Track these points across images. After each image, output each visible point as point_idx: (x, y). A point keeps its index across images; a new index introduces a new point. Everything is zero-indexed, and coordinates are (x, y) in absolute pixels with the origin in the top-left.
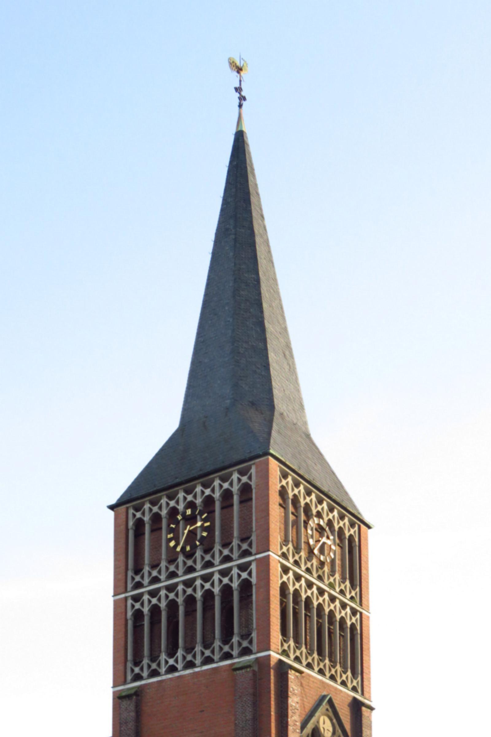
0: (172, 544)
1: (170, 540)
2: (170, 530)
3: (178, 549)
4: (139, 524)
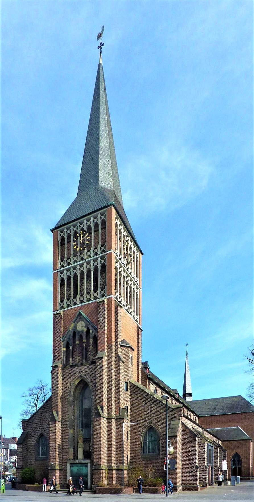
0: (75, 247)
1: (74, 245)
2: (74, 241)
3: (78, 250)
4: (63, 239)
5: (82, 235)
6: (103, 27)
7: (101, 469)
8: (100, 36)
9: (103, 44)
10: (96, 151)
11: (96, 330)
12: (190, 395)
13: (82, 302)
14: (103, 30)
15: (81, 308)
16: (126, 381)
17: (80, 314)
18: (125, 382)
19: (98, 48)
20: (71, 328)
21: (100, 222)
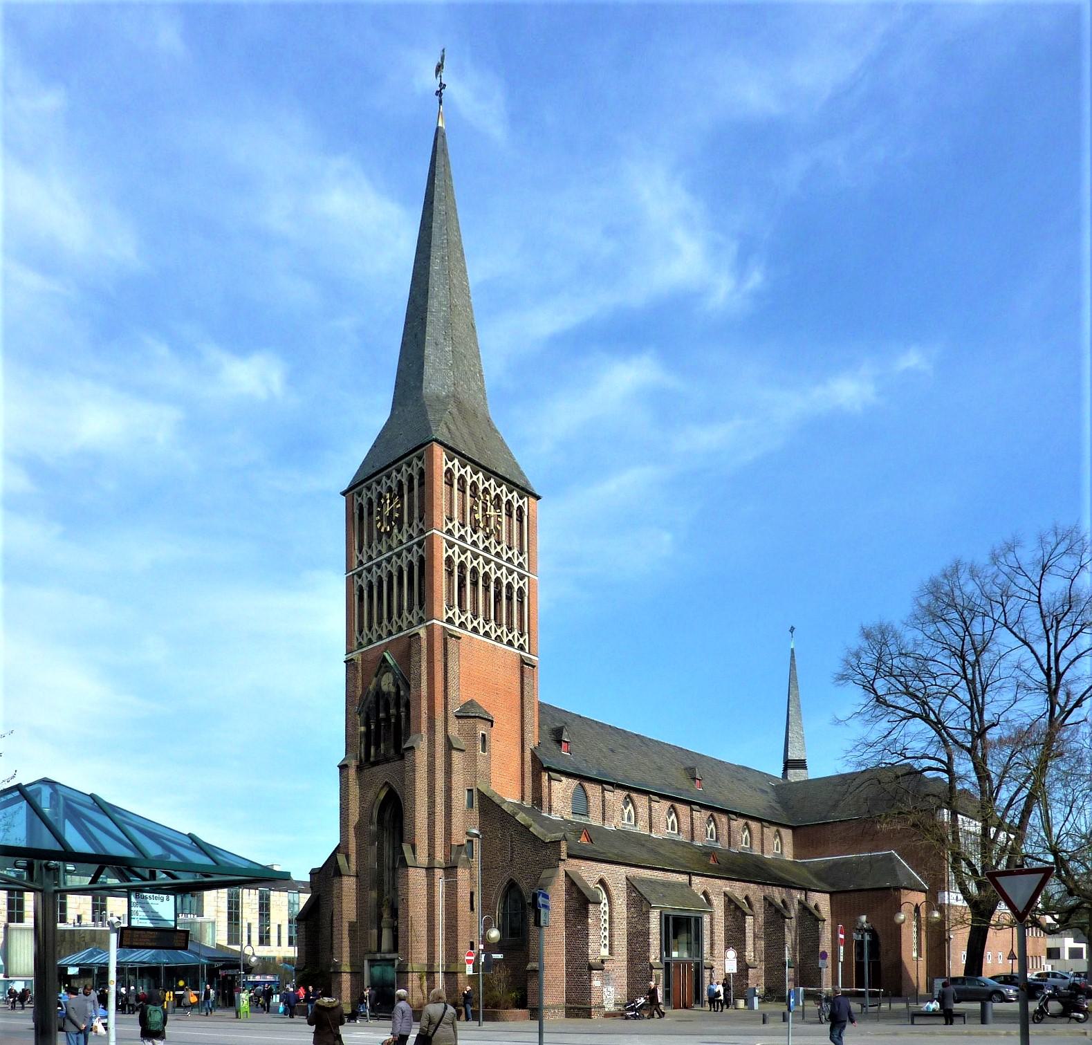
0: (379, 525)
1: (378, 521)
5: (388, 501)
6: (443, 51)
7: (408, 972)
9: (445, 85)
11: (408, 686)
12: (801, 764)
13: (390, 633)
14: (443, 58)
15: (386, 647)
16: (469, 788)
17: (385, 660)
18: (469, 790)
19: (436, 95)
20: (371, 687)
21: (407, 480)
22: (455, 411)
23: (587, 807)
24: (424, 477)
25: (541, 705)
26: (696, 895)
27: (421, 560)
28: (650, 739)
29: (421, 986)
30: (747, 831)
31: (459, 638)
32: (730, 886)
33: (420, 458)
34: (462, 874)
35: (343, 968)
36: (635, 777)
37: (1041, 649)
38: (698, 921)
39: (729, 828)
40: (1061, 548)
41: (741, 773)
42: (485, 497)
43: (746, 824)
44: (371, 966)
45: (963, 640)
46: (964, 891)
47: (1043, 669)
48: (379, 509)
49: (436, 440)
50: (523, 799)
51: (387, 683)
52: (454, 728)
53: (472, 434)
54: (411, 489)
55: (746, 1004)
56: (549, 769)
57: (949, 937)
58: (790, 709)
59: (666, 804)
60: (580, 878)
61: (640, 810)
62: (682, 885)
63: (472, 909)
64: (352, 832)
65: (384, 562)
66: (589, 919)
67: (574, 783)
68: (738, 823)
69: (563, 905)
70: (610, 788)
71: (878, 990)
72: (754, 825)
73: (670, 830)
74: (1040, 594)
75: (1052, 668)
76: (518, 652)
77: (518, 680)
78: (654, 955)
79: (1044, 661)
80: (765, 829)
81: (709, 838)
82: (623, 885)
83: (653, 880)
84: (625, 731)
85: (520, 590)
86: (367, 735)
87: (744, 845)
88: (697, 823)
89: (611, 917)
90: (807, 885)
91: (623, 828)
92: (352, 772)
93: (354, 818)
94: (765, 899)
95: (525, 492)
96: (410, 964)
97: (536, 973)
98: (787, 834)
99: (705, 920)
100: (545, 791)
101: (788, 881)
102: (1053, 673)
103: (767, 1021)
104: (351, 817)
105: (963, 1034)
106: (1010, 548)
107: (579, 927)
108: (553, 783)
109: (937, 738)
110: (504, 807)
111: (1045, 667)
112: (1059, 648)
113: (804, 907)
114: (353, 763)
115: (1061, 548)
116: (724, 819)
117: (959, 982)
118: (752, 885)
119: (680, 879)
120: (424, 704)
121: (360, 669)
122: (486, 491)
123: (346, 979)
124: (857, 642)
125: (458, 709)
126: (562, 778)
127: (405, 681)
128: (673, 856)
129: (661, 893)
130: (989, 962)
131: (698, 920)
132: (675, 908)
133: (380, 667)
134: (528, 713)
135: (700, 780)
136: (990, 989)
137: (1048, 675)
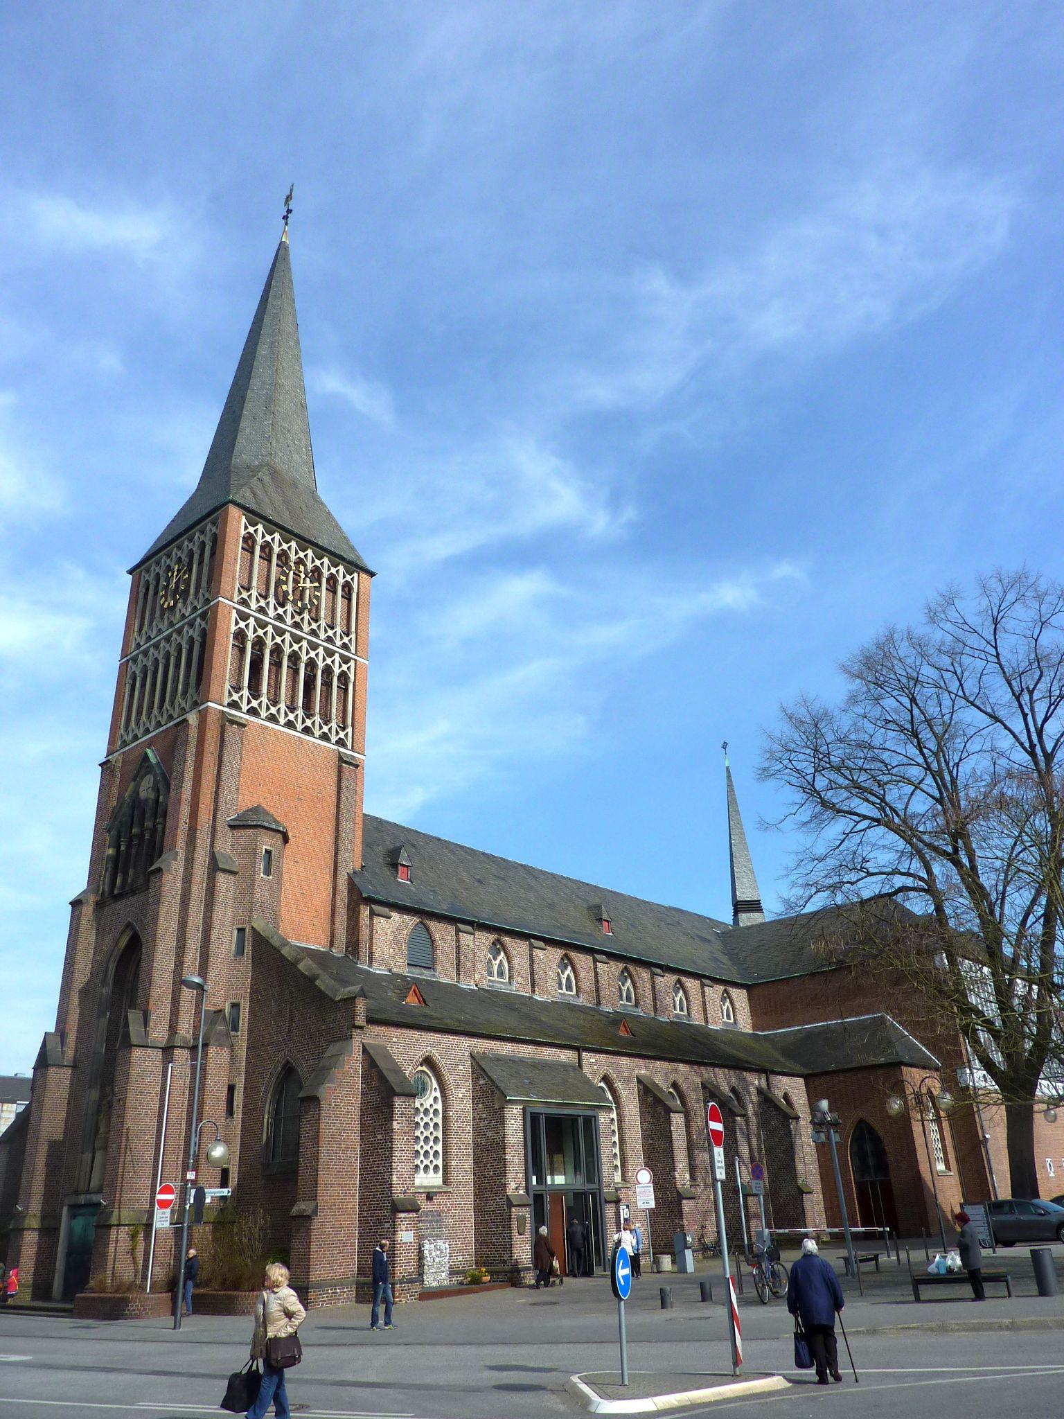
5: (175, 573)
6: (293, 186)
7: (110, 1226)
8: (289, 198)
10: (242, 397)
12: (755, 906)
15: (150, 744)
16: (240, 926)
17: (146, 757)
20: (127, 795)
22: (267, 479)
23: (434, 956)
24: (217, 545)
25: (365, 815)
26: (588, 1082)
27: (204, 634)
28: (541, 871)
29: (132, 1252)
30: (681, 992)
31: (244, 726)
32: (647, 1068)
33: (214, 523)
34: (217, 1056)
35: (27, 1221)
36: (509, 916)
37: (1018, 725)
38: (590, 1123)
39: (653, 986)
40: (1011, 597)
41: (674, 918)
42: (298, 568)
43: (679, 981)
44: (73, 1216)
45: (911, 712)
46: (988, 1065)
47: (1025, 748)
48: (165, 584)
49: (233, 502)
50: (332, 944)
51: (146, 789)
52: (225, 844)
53: (286, 502)
54: (201, 562)
55: (673, 1262)
56: (370, 901)
57: (984, 1137)
58: (732, 837)
59: (556, 954)
60: (388, 1056)
61: (516, 961)
62: (565, 1067)
63: (230, 1112)
64: (75, 998)
65: (163, 641)
66: (395, 1123)
67: (412, 921)
68: (666, 981)
69: (357, 1101)
70: (469, 928)
71: (881, 1229)
72: (691, 984)
73: (564, 991)
74: (998, 654)
75: (1036, 745)
76: (335, 747)
77: (334, 784)
78: (515, 1181)
79: (1024, 738)
80: (706, 989)
81: (624, 1002)
82: (465, 1066)
83: (517, 1060)
84: (505, 860)
85: (344, 677)
86: (116, 859)
87: (678, 1011)
88: (603, 980)
89: (445, 1119)
90: (768, 1066)
91: (490, 986)
92: (88, 911)
93: (83, 975)
94: (704, 1087)
95: (355, 566)
96: (116, 1212)
97: (305, 1220)
98: (740, 996)
99: (602, 1120)
100: (364, 932)
101: (739, 1060)
102: (1038, 750)
103: (668, 1301)
104: (76, 976)
105: (1001, 1328)
106: (950, 600)
107: (379, 1137)
108: (376, 920)
109: (909, 848)
110: (285, 951)
111: (1027, 745)
112: (1039, 724)
113: (766, 1098)
114: (92, 898)
115: (1011, 597)
116: (645, 974)
117: (1006, 1209)
118: (681, 1065)
119: (563, 1057)
120: (185, 810)
121: (118, 774)
122: (300, 562)
123: (30, 1241)
124: (783, 729)
125: (233, 817)
126: (393, 914)
127: (166, 782)
128: (562, 1024)
129: (527, 1079)
130: (1052, 1175)
131: (591, 1120)
132: (547, 1102)
133: (140, 768)
134: (345, 826)
135: (608, 921)
136: (1053, 1219)
137: (1032, 754)
